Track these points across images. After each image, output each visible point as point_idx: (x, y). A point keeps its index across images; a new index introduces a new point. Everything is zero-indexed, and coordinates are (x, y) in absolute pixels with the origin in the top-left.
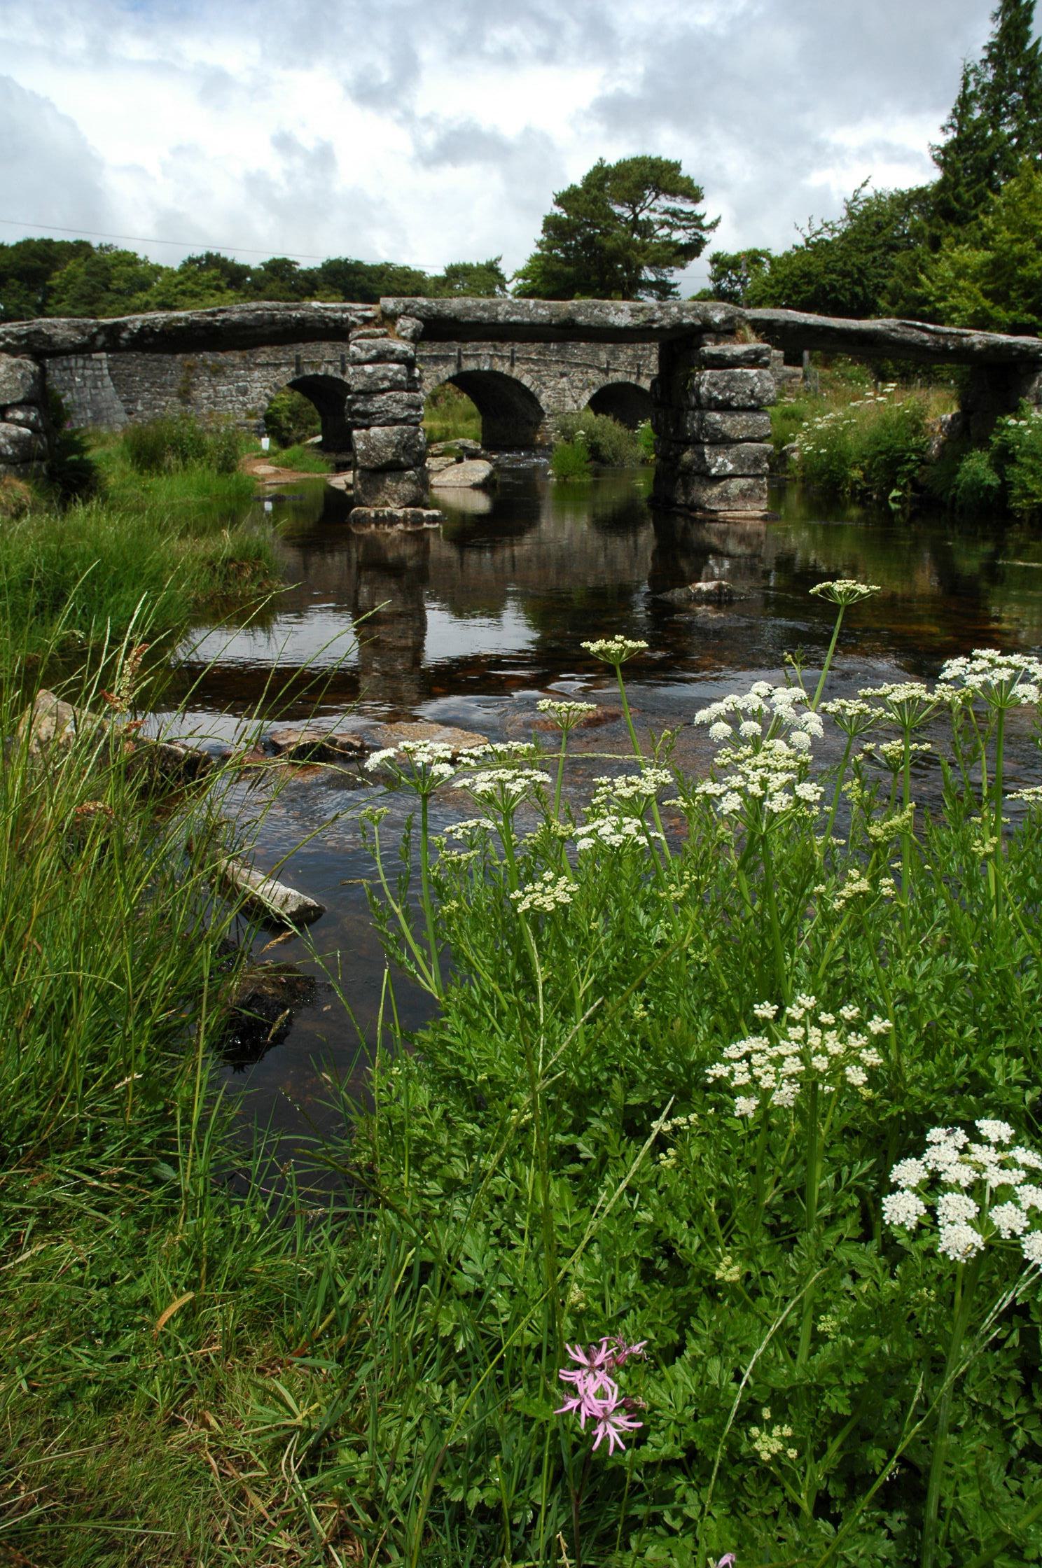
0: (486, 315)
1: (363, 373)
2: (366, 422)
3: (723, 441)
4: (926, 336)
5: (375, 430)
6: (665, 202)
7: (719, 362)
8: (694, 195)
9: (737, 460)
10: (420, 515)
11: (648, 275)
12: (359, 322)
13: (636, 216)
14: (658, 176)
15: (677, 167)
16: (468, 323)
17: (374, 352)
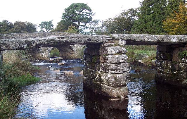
1: (115, 57)
2: (113, 72)
6: (84, 11)
8: (90, 10)
11: (81, 24)
12: (107, 41)
13: (79, 13)
14: (84, 7)
15: (87, 5)
16: (137, 41)
17: (118, 51)
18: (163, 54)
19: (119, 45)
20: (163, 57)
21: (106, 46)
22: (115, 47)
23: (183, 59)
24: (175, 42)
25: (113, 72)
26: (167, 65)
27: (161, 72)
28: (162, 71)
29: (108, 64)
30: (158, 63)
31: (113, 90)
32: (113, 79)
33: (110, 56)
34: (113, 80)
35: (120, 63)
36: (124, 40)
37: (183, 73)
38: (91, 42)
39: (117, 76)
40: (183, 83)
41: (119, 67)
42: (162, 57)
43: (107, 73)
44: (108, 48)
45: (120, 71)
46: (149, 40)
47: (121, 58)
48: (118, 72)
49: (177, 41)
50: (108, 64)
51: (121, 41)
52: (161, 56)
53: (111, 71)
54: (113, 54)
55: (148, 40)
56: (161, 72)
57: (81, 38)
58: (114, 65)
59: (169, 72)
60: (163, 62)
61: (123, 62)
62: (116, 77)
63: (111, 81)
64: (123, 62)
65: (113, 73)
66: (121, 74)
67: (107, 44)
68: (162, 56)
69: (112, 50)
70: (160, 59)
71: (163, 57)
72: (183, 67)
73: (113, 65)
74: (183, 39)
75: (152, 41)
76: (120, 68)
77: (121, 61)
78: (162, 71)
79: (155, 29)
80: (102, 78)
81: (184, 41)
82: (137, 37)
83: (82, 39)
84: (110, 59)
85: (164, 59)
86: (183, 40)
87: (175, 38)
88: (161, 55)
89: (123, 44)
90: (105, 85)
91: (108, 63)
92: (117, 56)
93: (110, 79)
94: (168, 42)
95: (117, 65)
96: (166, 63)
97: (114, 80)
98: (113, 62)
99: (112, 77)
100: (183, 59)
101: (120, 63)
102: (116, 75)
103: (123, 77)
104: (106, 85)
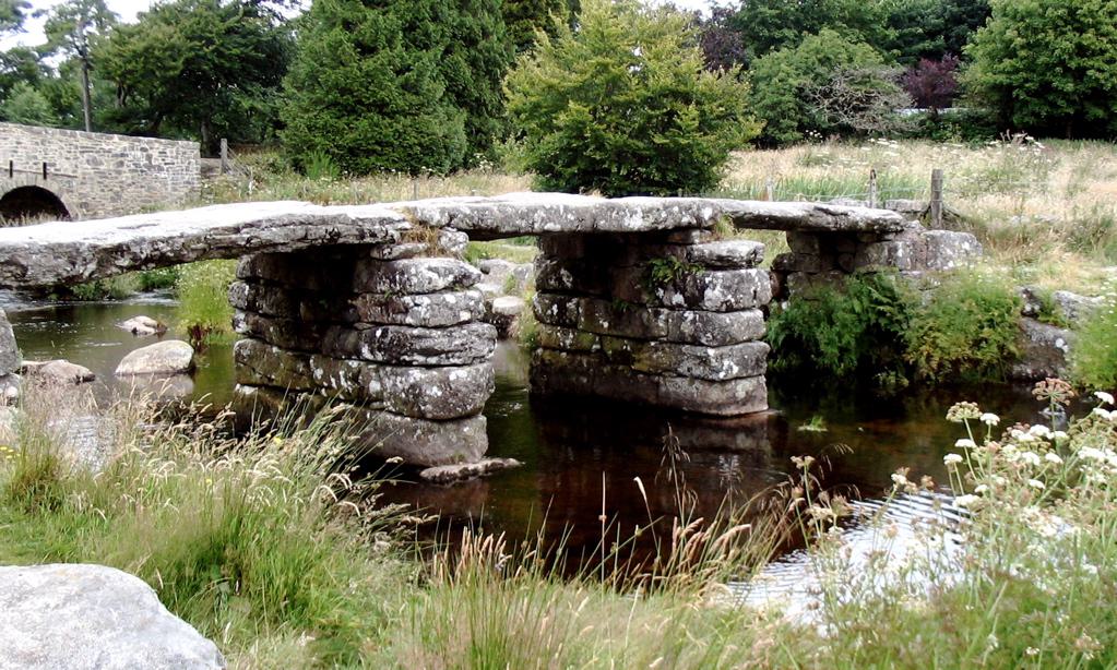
0: (524, 224)
2: (433, 360)
3: (726, 340)
4: (830, 218)
5: (456, 374)
7: (725, 263)
9: (742, 363)
10: (466, 469)
19: (443, 252)
20: (569, 285)
21: (395, 259)
22: (436, 262)
24: (636, 228)
25: (433, 360)
26: (960, 451)
27: (562, 349)
28: (568, 342)
29: (415, 332)
30: (550, 307)
31: (432, 432)
32: (435, 389)
33: (425, 300)
34: (435, 391)
35: (461, 324)
36: (459, 230)
39: (452, 377)
40: (663, 389)
41: (457, 342)
42: (568, 281)
43: (409, 364)
45: (459, 358)
47: (462, 304)
48: (452, 361)
50: (415, 332)
51: (450, 235)
52: (559, 279)
53: (421, 359)
54: (434, 292)
55: (546, 228)
57: (305, 227)
60: (571, 305)
63: (427, 399)
64: (468, 322)
65: (429, 367)
66: (468, 368)
68: (565, 279)
69: (431, 274)
71: (569, 285)
73: (435, 333)
74: (664, 215)
75: (558, 227)
76: (462, 345)
77: (465, 316)
78: (568, 342)
79: (313, 85)
80: (374, 386)
81: (667, 223)
83: (307, 230)
84: (422, 310)
85: (570, 293)
87: (636, 212)
88: (563, 271)
89: (461, 246)
90: (389, 416)
92: (450, 298)
94: (613, 229)
96: (586, 310)
97: (440, 393)
98: (432, 323)
101: (461, 324)
102: (449, 372)
103: (475, 378)
104: (396, 414)
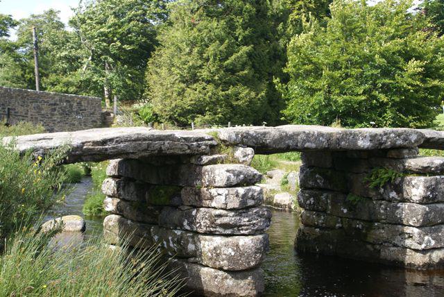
2: (229, 232)
18: (324, 175)
23: (382, 190)
24: (366, 147)
25: (229, 232)
27: (317, 226)
30: (308, 199)
32: (230, 250)
34: (230, 251)
37: (383, 228)
38: (382, 147)
44: (411, 179)
46: (307, 145)
49: (371, 144)
50: (218, 212)
56: (317, 226)
58: (233, 213)
59: (340, 225)
60: (323, 197)
61: (253, 206)
62: (237, 246)
64: (253, 206)
66: (251, 237)
67: (205, 159)
70: (312, 188)
72: (382, 211)
74: (384, 138)
75: (314, 146)
77: (251, 203)
82: (344, 136)
85: (322, 190)
86: (386, 142)
88: (317, 176)
91: (215, 208)
92: (241, 190)
93: (222, 249)
95: (241, 213)
99: (226, 245)
100: (382, 190)
